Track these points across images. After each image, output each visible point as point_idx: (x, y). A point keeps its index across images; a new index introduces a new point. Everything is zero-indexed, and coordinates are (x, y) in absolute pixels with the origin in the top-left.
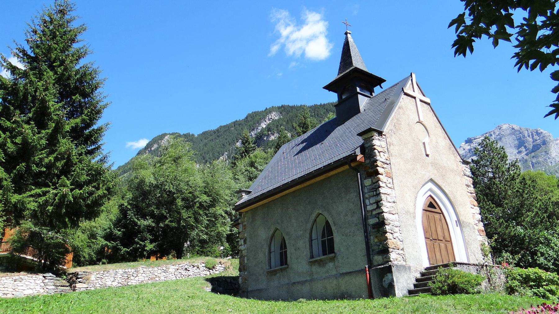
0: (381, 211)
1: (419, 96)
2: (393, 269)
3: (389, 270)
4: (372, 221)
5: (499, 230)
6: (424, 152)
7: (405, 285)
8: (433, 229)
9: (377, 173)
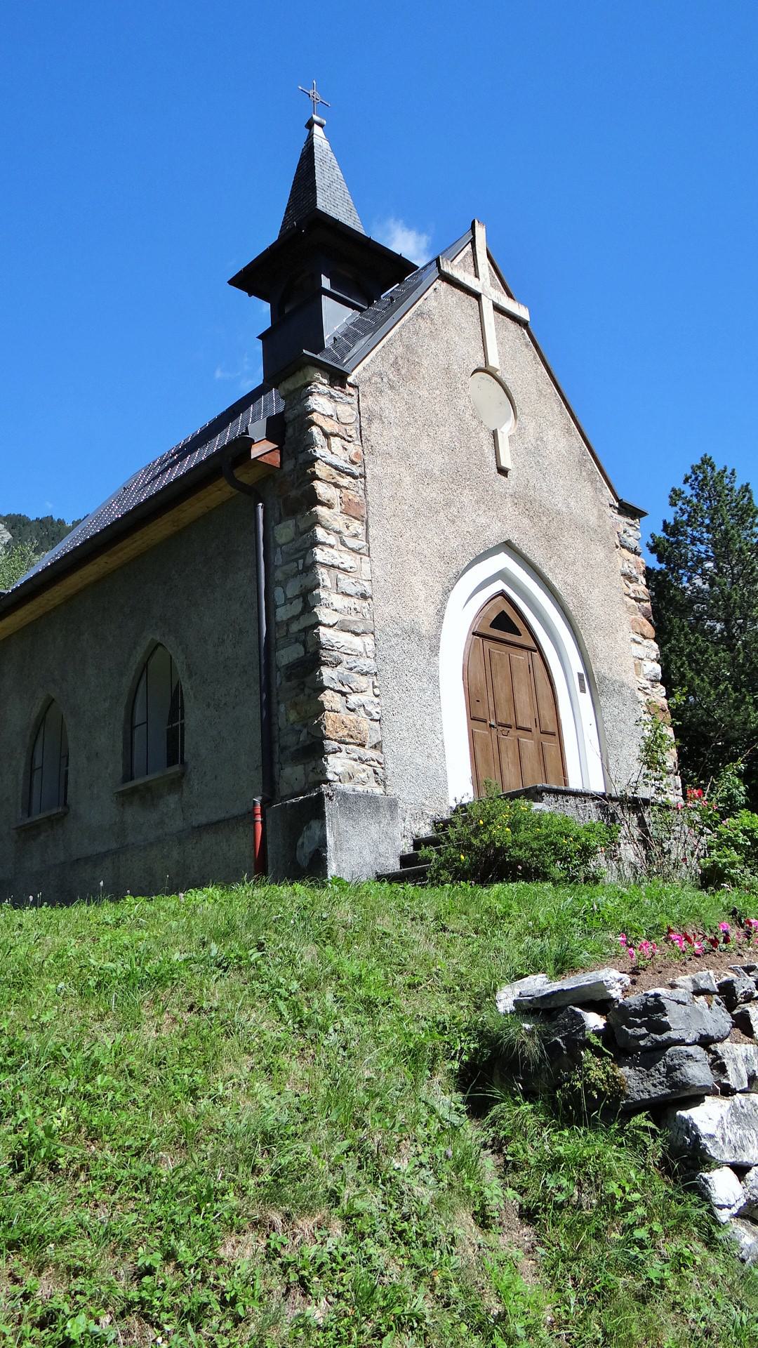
0: (313, 621)
1: (493, 294)
2: (330, 807)
3: (314, 810)
4: (287, 655)
5: (718, 713)
6: (492, 458)
7: (369, 858)
8: (503, 694)
9: (314, 500)
